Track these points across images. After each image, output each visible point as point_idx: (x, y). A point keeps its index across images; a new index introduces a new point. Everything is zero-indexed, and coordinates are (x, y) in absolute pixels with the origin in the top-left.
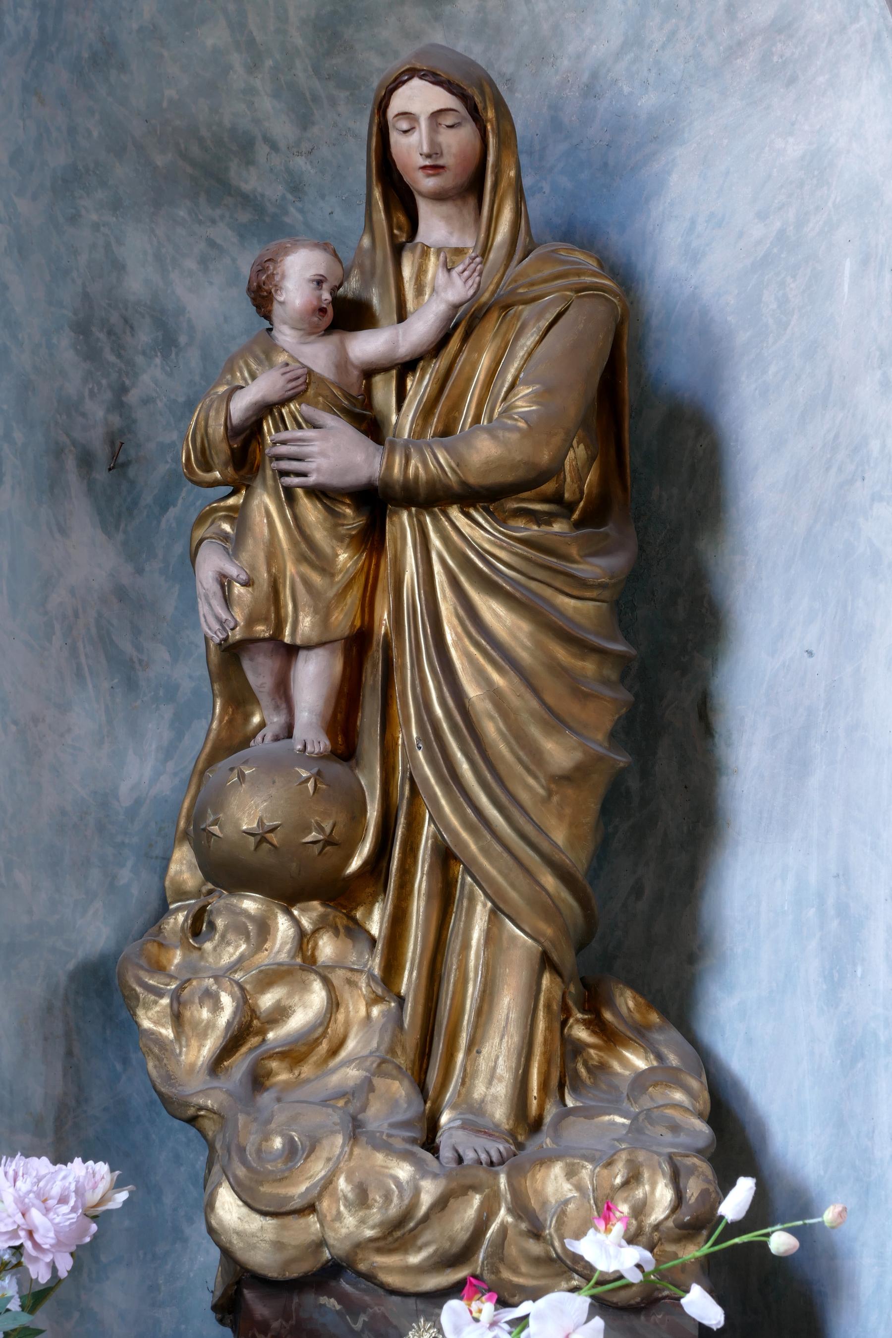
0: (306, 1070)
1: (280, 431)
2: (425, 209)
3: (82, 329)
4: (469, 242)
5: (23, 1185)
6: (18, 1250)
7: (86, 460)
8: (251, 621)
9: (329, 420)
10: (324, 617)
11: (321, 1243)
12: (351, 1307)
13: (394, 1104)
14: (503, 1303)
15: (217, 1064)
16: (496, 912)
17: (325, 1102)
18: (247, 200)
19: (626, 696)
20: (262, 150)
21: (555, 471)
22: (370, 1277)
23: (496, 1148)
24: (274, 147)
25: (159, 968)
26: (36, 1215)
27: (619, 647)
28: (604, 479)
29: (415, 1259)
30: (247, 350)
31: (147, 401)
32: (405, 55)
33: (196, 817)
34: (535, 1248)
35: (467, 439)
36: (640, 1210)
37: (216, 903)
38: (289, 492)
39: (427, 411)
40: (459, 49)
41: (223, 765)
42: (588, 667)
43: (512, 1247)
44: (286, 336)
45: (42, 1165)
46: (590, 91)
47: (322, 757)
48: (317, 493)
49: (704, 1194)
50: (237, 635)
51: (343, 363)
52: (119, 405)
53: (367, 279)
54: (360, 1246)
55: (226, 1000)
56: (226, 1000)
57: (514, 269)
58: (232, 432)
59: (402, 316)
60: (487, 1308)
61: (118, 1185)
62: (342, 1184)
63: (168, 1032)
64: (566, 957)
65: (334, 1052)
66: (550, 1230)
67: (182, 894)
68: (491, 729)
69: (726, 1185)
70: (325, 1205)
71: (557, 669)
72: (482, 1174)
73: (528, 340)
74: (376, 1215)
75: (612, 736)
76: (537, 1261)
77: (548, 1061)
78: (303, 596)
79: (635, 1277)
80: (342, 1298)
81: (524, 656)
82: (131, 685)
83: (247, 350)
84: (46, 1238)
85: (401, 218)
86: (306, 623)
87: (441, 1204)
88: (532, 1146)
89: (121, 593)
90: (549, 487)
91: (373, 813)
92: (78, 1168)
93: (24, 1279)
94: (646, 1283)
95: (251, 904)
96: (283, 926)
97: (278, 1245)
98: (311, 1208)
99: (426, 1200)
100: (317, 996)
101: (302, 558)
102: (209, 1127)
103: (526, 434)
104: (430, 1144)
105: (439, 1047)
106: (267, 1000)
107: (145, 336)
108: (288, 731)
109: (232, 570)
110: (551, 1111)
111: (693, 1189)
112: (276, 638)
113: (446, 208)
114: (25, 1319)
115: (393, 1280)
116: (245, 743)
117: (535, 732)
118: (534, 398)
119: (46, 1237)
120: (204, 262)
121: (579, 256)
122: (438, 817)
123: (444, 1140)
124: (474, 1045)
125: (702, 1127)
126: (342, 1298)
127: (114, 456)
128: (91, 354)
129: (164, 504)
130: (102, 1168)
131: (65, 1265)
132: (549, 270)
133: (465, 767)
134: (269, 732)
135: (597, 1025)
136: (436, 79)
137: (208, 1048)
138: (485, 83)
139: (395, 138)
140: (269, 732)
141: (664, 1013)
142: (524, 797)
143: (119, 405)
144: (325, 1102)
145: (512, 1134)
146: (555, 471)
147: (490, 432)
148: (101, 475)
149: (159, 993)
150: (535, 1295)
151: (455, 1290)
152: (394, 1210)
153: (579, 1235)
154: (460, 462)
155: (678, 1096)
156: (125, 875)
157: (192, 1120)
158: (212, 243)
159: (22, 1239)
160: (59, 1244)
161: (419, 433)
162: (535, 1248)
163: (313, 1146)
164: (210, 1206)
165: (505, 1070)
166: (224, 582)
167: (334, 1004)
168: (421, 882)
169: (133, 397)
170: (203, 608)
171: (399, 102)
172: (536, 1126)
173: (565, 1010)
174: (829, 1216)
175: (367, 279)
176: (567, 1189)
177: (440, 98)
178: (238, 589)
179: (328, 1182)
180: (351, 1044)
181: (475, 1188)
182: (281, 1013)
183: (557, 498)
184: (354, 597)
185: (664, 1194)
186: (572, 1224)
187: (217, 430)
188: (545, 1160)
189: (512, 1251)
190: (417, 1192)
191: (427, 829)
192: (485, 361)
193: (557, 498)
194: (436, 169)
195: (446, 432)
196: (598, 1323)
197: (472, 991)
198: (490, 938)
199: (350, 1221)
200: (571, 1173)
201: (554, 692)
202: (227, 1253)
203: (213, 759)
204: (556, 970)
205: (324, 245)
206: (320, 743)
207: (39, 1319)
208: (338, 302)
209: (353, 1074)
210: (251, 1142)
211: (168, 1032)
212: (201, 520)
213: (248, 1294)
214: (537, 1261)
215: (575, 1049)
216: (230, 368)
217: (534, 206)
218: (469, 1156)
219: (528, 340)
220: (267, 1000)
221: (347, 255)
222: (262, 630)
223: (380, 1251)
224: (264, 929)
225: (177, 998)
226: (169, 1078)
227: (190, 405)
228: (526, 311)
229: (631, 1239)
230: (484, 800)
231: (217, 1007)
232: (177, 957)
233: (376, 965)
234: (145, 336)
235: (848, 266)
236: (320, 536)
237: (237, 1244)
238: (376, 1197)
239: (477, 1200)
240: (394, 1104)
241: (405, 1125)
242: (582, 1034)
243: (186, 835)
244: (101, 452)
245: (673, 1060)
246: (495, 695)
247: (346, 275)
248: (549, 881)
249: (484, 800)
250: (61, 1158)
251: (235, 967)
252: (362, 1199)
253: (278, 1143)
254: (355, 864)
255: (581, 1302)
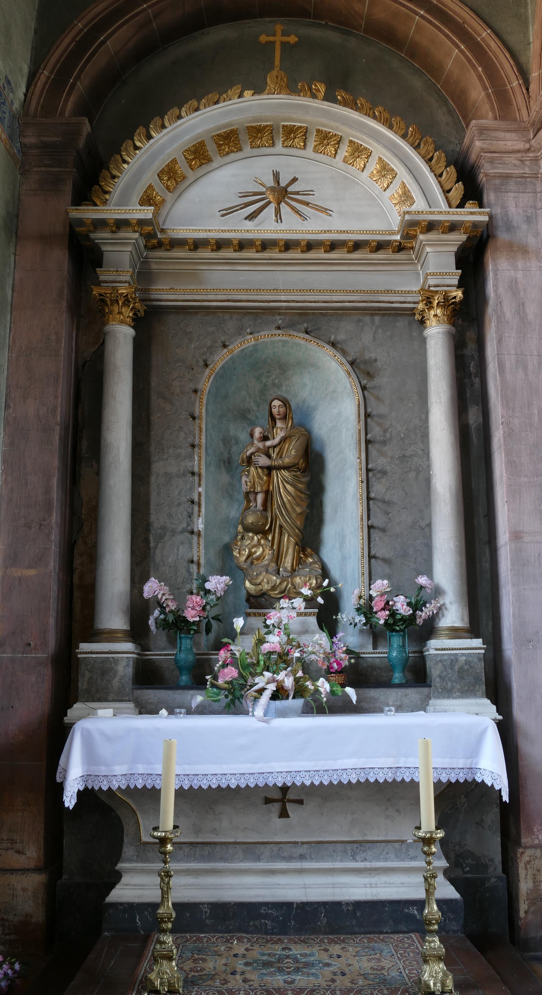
0: (259, 562)
1: (209, 160)
2: (277, 421)
3: (223, 440)
4: (284, 426)
5: (216, 580)
6: (215, 591)
7: (224, 462)
8: (250, 488)
9: (262, 455)
10: (262, 488)
11: (262, 590)
12: (266, 600)
13: (273, 567)
14: (290, 600)
15: (246, 561)
16: (289, 536)
17: (262, 567)
18: (249, 420)
19: (309, 500)
20: (251, 411)
21: (298, 464)
22: (269, 595)
23: (289, 574)
24: (253, 411)
25: (236, 545)
26: (218, 585)
27: (308, 493)
28: (306, 466)
29: (276, 592)
30: (249, 444)
31: (234, 452)
32: (274, 396)
33: (242, 520)
34: (295, 590)
35: (284, 458)
36: (311, 584)
37: (245, 534)
38: (256, 467)
39: (278, 454)
40: (283, 395)
41: (246, 512)
42: (303, 496)
43: (325, 699)
44: (256, 442)
45: (219, 577)
46: (304, 402)
47: (262, 510)
48: (260, 467)
49: (321, 582)
50: (248, 490)
51: (264, 446)
52: (229, 453)
53: (268, 433)
54: (268, 590)
55: (247, 550)
56: (247, 550)
57: (292, 431)
58: (247, 457)
59: (274, 438)
60: (287, 600)
61: (230, 580)
62: (265, 580)
63: (238, 555)
64: (300, 543)
65: (264, 559)
66: (297, 588)
67: (240, 533)
68: (288, 506)
69: (324, 580)
70: (262, 584)
71: (298, 496)
72: (286, 579)
73: (294, 443)
74: (270, 585)
75: (307, 507)
76: (295, 593)
77: (297, 560)
78: (258, 484)
79: (310, 595)
80: (265, 599)
81: (293, 494)
82: (232, 499)
83: (249, 444)
84: (220, 589)
85: (274, 422)
86: (259, 488)
87: (280, 583)
88: (294, 574)
89: (230, 484)
90: (297, 466)
91: (269, 520)
92: (224, 577)
93: (216, 596)
94: (312, 596)
95: (250, 535)
96: (256, 537)
97: (255, 590)
98: (260, 584)
99: (278, 583)
100: (261, 549)
101: (258, 478)
102: (245, 571)
103: (294, 458)
104: (278, 574)
105: (280, 558)
106: (253, 550)
107: (233, 442)
108: (256, 506)
109: (247, 480)
110: (297, 568)
111: (319, 581)
112: (254, 491)
113: (281, 421)
114: (216, 602)
115: (273, 596)
116: (249, 508)
117: (295, 506)
118: (295, 452)
119: (220, 589)
120: (243, 430)
121: (302, 429)
122: (280, 520)
123: (281, 573)
124: (285, 557)
125: (320, 571)
126: (265, 599)
127: (229, 461)
128: (225, 445)
129: (237, 469)
130: (228, 577)
131: (222, 593)
132: (297, 431)
133: (284, 512)
134: (253, 506)
135: (304, 554)
136: (279, 400)
137: (244, 558)
138: (287, 401)
139: (273, 409)
140: (253, 506)
141: (315, 552)
142: (293, 517)
143: (229, 453)
144: (262, 567)
145: (291, 572)
146: (298, 464)
147: (288, 457)
148: (227, 465)
149: (237, 549)
150: (295, 598)
151: (282, 597)
152: (273, 584)
153: (301, 589)
154: (283, 462)
155: (317, 566)
156: (231, 530)
157: (242, 570)
158: (244, 427)
159: (216, 589)
160: (221, 590)
161: (277, 457)
162: (295, 590)
163: (260, 574)
164: (245, 584)
165: (290, 561)
166: (246, 482)
167: (264, 551)
168: (277, 531)
169: (231, 452)
170: (243, 486)
171: (273, 404)
172: (295, 571)
173: (299, 552)
174: (340, 585)
175: (268, 433)
176: (300, 581)
177: (280, 403)
178: (248, 483)
179: (263, 580)
180: (266, 557)
181: (285, 581)
182: (255, 552)
183: (298, 468)
184: (266, 484)
185: (314, 582)
186: (300, 587)
187: (245, 457)
188: (296, 576)
189: (291, 591)
190: (276, 581)
191: (278, 522)
192: (287, 446)
193: (298, 468)
194: (279, 415)
195: (281, 457)
196: (304, 603)
197: (285, 549)
198: (288, 540)
199: (266, 586)
200: (300, 578)
201: (298, 500)
202: (247, 591)
203: (245, 511)
204: (298, 545)
205: (261, 427)
206: (261, 508)
207: (219, 602)
208: (264, 436)
209: (267, 562)
210: (251, 573)
211: (238, 555)
212: (242, 472)
213: (251, 598)
214: (295, 593)
215: (301, 558)
216: (247, 447)
217: (295, 421)
218: (284, 576)
219: (294, 443)
220: (253, 550)
221: (265, 429)
222: (252, 490)
223: (271, 591)
224: (253, 538)
225: (239, 550)
226: (238, 563)
227: (240, 453)
228: (293, 438)
229: (309, 589)
230: (287, 517)
231: (245, 551)
232: (239, 543)
233: (270, 544)
234: (233, 442)
235: (344, 430)
236: (261, 474)
237: (249, 590)
238: (270, 582)
239: (286, 583)
240: (273, 567)
241: (275, 570)
242: (302, 556)
243: (240, 523)
244: (227, 461)
245: (316, 560)
246: (289, 500)
247: (265, 432)
248: (297, 531)
249: (287, 517)
250: (222, 576)
251: (248, 545)
252: (268, 583)
253: (255, 573)
254: (267, 528)
255: (302, 599)
